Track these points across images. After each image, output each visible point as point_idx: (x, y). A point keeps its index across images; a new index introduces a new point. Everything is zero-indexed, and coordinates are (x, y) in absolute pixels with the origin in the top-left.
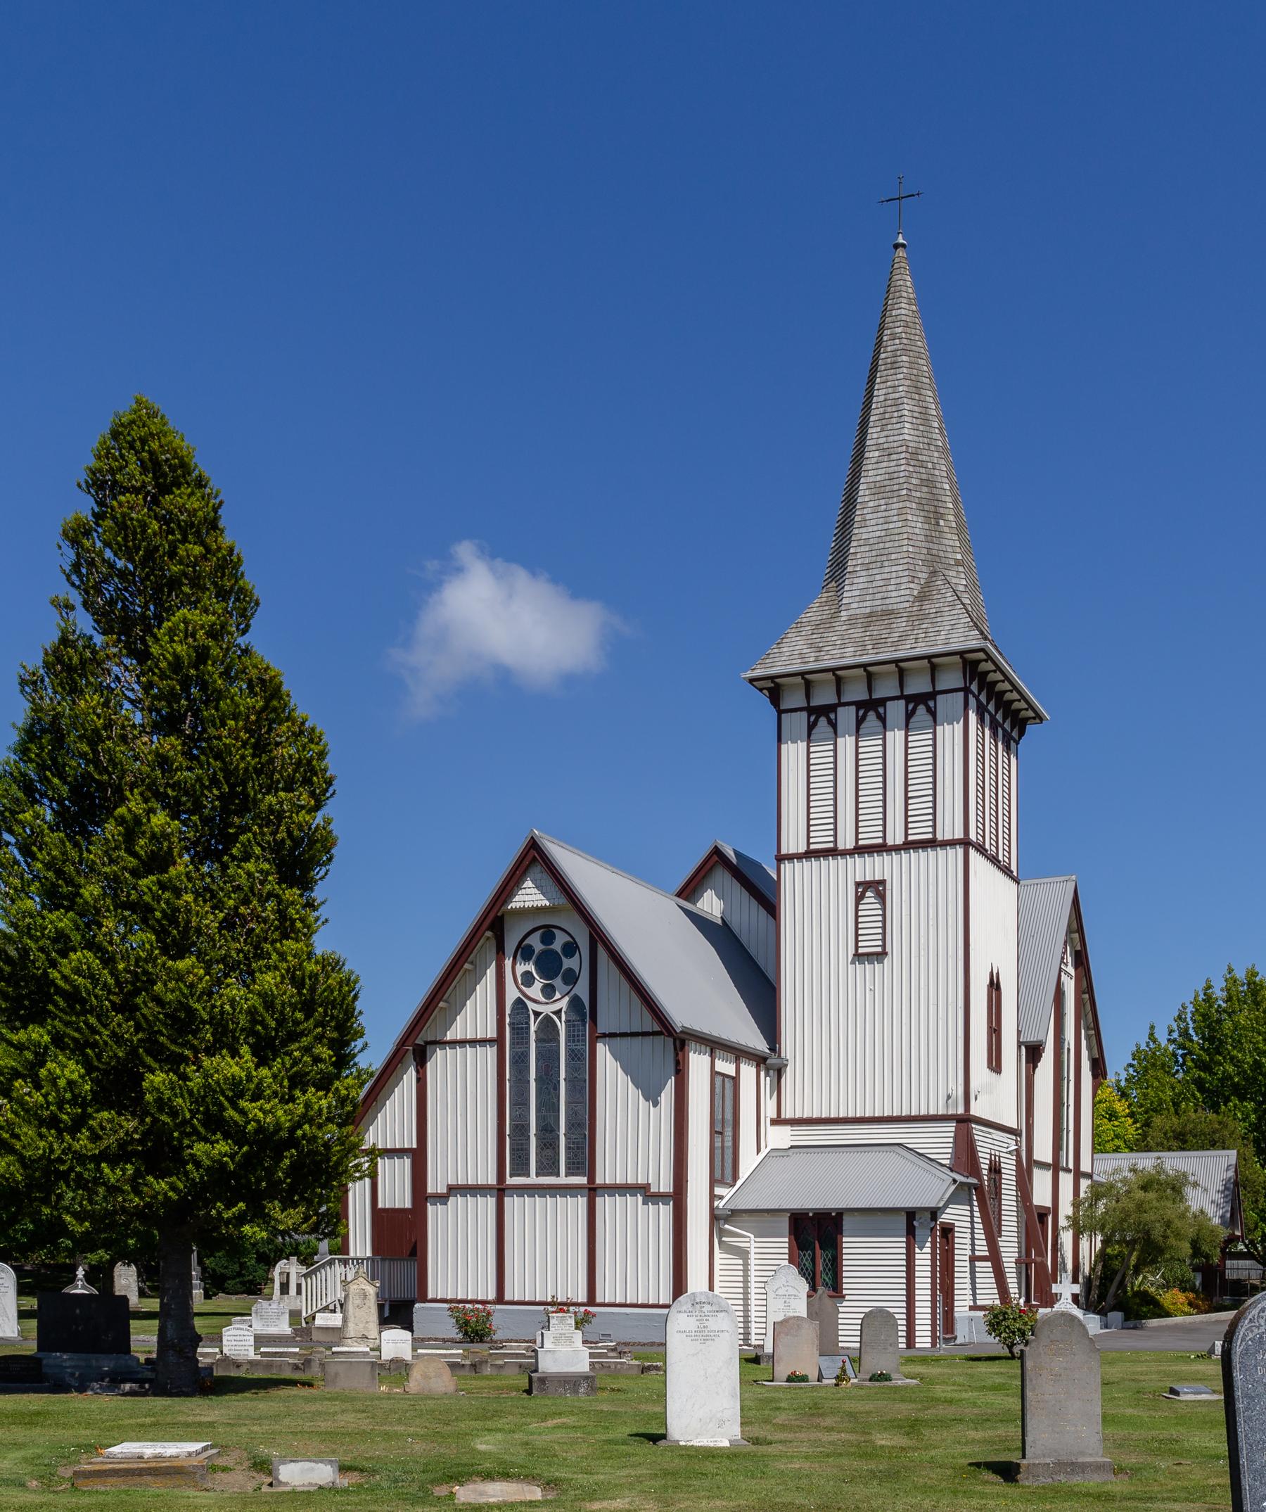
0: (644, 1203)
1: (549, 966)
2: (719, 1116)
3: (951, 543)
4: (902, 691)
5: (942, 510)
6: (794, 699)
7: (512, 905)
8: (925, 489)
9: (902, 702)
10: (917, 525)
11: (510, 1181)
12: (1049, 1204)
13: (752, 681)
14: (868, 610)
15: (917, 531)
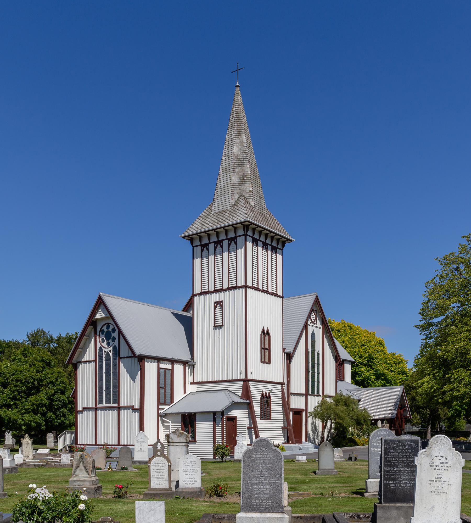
0: (132, 412)
1: (108, 336)
2: (162, 382)
3: (248, 185)
4: (227, 237)
5: (246, 174)
6: (197, 243)
7: (96, 317)
8: (240, 168)
9: (227, 241)
10: (236, 180)
12: (304, 407)
13: (183, 237)
14: (219, 211)
15: (236, 182)
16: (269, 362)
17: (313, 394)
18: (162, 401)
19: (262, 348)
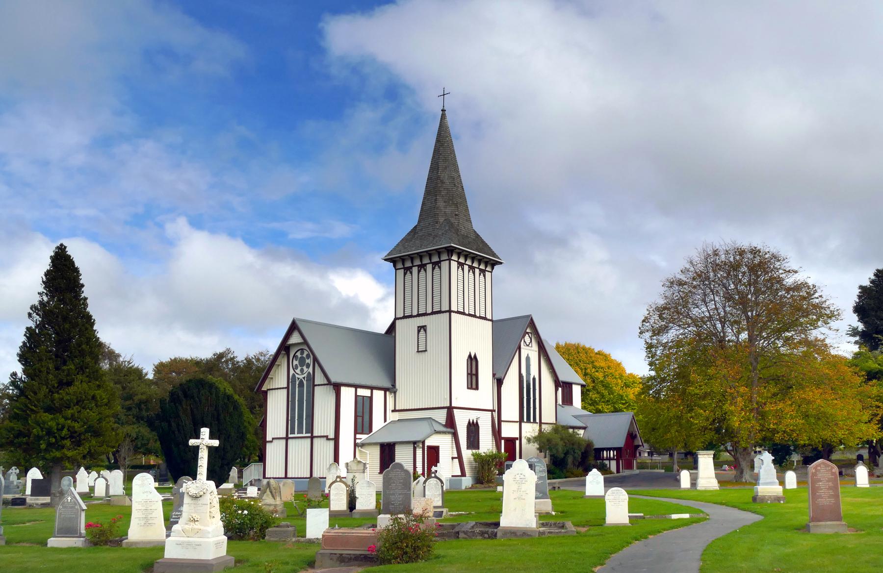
11: (290, 436)
12: (518, 436)
16: (477, 388)
17: (528, 421)
18: (359, 430)
19: (468, 374)
